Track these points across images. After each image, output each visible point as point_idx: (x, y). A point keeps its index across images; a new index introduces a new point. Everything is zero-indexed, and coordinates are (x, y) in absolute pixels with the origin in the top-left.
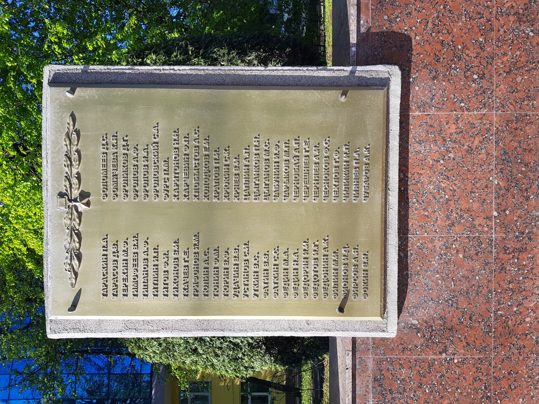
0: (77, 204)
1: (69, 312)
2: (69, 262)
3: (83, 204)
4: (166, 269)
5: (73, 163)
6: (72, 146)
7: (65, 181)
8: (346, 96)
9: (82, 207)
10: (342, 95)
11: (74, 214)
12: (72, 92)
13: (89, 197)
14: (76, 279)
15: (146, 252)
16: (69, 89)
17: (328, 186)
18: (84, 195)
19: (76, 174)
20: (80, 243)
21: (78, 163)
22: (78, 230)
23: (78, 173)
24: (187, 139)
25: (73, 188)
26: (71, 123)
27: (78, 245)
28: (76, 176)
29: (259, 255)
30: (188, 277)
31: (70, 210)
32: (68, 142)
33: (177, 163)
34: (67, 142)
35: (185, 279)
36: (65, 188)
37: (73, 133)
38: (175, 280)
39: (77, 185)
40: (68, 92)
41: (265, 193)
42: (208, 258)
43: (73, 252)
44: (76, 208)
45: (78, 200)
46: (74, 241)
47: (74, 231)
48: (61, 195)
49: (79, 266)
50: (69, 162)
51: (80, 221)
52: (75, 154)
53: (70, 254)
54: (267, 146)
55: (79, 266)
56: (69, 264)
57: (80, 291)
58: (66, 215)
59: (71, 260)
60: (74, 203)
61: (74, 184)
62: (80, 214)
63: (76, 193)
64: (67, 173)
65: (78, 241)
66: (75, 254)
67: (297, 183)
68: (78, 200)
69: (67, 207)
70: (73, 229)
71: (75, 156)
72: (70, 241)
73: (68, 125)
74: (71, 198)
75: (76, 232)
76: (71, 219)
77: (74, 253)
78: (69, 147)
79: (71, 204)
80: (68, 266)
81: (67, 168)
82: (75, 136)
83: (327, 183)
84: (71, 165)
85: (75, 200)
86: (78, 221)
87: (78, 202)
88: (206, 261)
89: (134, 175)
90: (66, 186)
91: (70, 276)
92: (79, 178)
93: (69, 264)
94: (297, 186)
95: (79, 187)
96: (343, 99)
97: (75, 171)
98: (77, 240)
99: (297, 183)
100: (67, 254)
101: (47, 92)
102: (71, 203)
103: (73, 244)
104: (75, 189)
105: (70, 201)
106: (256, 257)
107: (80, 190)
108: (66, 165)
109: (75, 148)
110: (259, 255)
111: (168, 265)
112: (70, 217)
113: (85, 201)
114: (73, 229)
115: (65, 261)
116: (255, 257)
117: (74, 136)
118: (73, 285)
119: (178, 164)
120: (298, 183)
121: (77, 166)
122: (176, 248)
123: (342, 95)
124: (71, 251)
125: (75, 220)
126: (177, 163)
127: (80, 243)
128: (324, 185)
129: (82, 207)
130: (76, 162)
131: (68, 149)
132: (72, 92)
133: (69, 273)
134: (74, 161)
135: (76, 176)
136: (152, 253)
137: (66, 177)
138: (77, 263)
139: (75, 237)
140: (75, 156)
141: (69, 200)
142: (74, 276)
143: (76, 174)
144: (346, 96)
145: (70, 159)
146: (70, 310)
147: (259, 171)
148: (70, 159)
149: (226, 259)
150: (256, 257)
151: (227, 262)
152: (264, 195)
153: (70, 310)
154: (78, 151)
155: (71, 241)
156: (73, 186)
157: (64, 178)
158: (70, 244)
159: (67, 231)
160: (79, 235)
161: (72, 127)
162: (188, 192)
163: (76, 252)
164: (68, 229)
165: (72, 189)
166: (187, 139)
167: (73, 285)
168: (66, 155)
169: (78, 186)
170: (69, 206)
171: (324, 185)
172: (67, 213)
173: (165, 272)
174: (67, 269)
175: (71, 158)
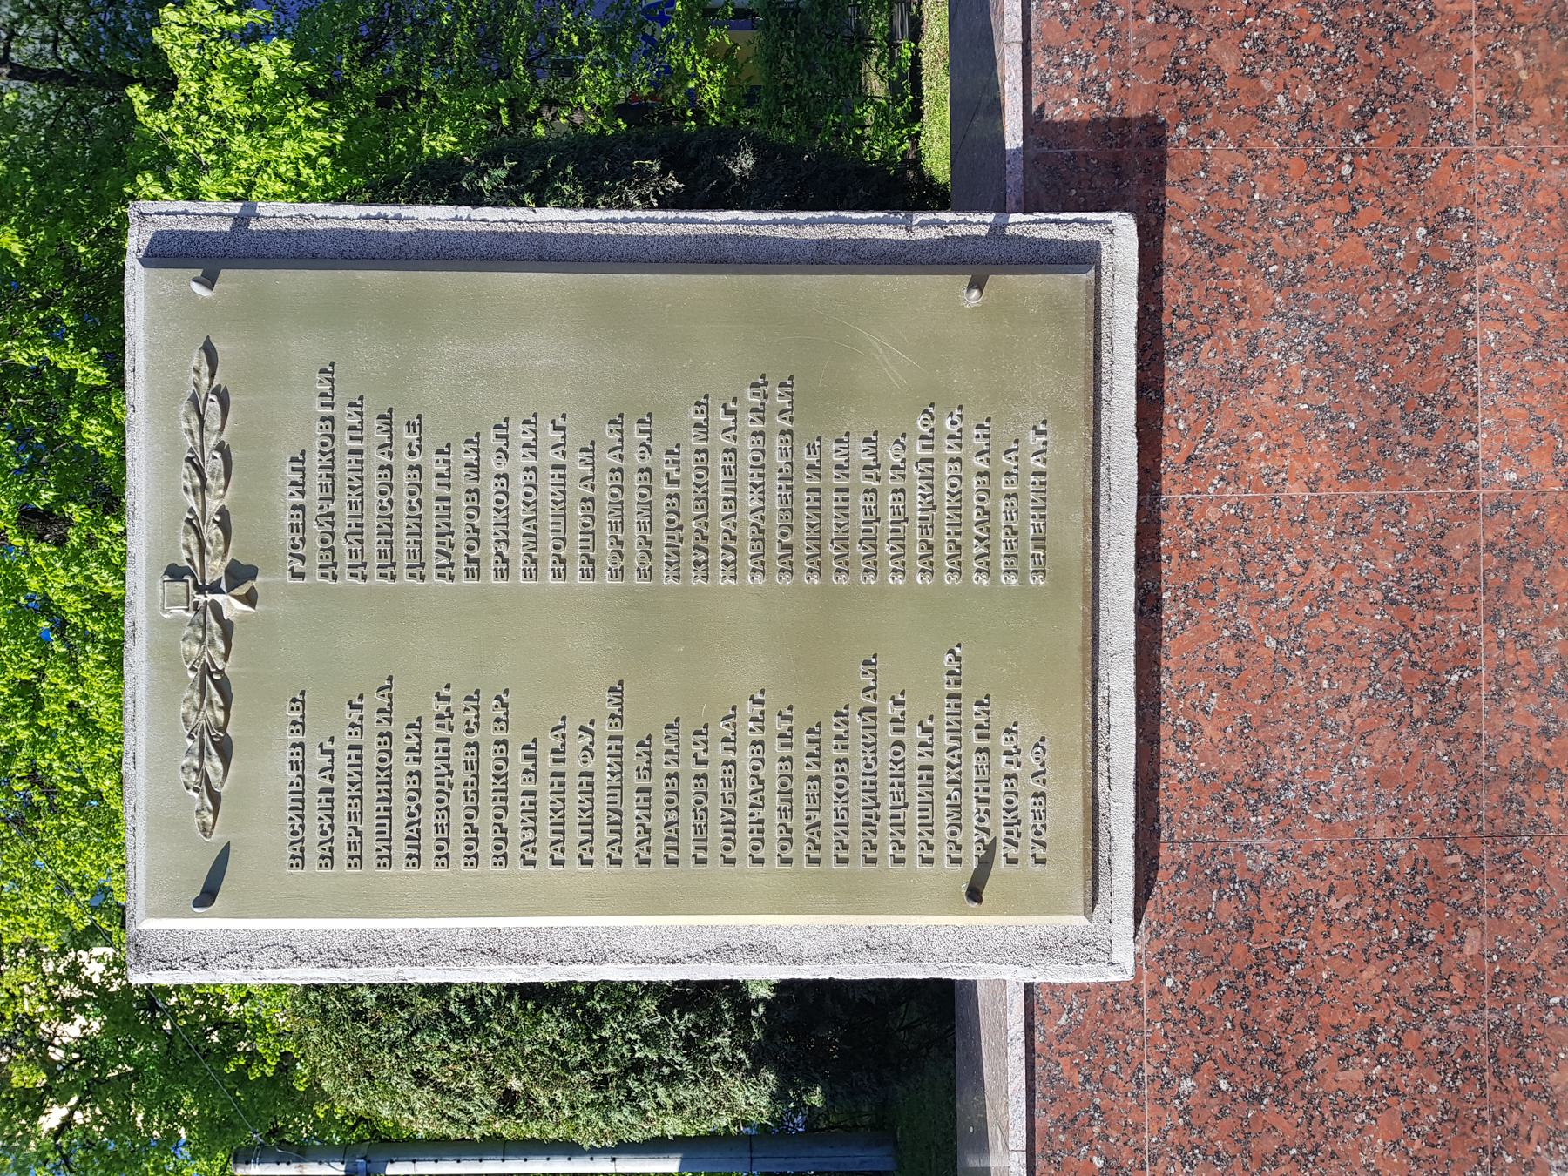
0: (219, 598)
1: (196, 910)
2: (197, 764)
5: (209, 481)
6: (205, 434)
7: (186, 532)
8: (981, 291)
9: (232, 607)
10: (970, 287)
13: (254, 578)
14: (215, 813)
16: (198, 273)
18: (238, 575)
20: (226, 709)
21: (222, 481)
22: (221, 672)
23: (222, 512)
25: (208, 554)
26: (205, 368)
27: (220, 715)
28: (218, 519)
31: (200, 615)
32: (195, 423)
36: (185, 554)
37: (211, 397)
39: (218, 544)
43: (206, 734)
44: (217, 609)
45: (223, 586)
46: (211, 703)
48: (175, 573)
49: (225, 776)
50: (197, 481)
51: (228, 646)
52: (214, 457)
53: (197, 744)
55: (225, 776)
56: (195, 770)
57: (227, 848)
58: (187, 631)
60: (210, 597)
61: (211, 541)
62: (227, 629)
63: (215, 569)
64: (191, 511)
65: (221, 704)
66: (213, 742)
68: (223, 586)
69: (191, 605)
70: (207, 671)
71: (214, 464)
72: (198, 704)
74: (203, 581)
75: (216, 677)
76: (201, 642)
77: (212, 738)
78: (197, 435)
79: (201, 599)
80: (194, 777)
82: (216, 405)
84: (204, 486)
85: (215, 588)
86: (221, 645)
87: (223, 592)
91: (198, 805)
92: (224, 524)
93: (195, 770)
97: (213, 505)
98: (217, 699)
100: (190, 742)
102: (202, 596)
103: (209, 713)
104: (216, 557)
105: (200, 589)
108: (190, 488)
109: (212, 441)
112: (200, 634)
113: (242, 590)
114: (207, 671)
117: (213, 407)
121: (221, 492)
123: (970, 287)
124: (202, 733)
125: (212, 644)
127: (226, 709)
129: (232, 607)
130: (218, 479)
132: (209, 281)
133: (196, 795)
135: (218, 519)
138: (219, 766)
139: (214, 691)
140: (214, 464)
141: (196, 585)
144: (981, 291)
146: (198, 903)
154: (221, 448)
155: (201, 705)
156: (208, 545)
159: (192, 675)
160: (224, 688)
161: (207, 380)
163: (217, 736)
164: (192, 669)
165: (206, 557)
168: (189, 460)
169: (221, 548)
170: (196, 604)
174: (191, 784)
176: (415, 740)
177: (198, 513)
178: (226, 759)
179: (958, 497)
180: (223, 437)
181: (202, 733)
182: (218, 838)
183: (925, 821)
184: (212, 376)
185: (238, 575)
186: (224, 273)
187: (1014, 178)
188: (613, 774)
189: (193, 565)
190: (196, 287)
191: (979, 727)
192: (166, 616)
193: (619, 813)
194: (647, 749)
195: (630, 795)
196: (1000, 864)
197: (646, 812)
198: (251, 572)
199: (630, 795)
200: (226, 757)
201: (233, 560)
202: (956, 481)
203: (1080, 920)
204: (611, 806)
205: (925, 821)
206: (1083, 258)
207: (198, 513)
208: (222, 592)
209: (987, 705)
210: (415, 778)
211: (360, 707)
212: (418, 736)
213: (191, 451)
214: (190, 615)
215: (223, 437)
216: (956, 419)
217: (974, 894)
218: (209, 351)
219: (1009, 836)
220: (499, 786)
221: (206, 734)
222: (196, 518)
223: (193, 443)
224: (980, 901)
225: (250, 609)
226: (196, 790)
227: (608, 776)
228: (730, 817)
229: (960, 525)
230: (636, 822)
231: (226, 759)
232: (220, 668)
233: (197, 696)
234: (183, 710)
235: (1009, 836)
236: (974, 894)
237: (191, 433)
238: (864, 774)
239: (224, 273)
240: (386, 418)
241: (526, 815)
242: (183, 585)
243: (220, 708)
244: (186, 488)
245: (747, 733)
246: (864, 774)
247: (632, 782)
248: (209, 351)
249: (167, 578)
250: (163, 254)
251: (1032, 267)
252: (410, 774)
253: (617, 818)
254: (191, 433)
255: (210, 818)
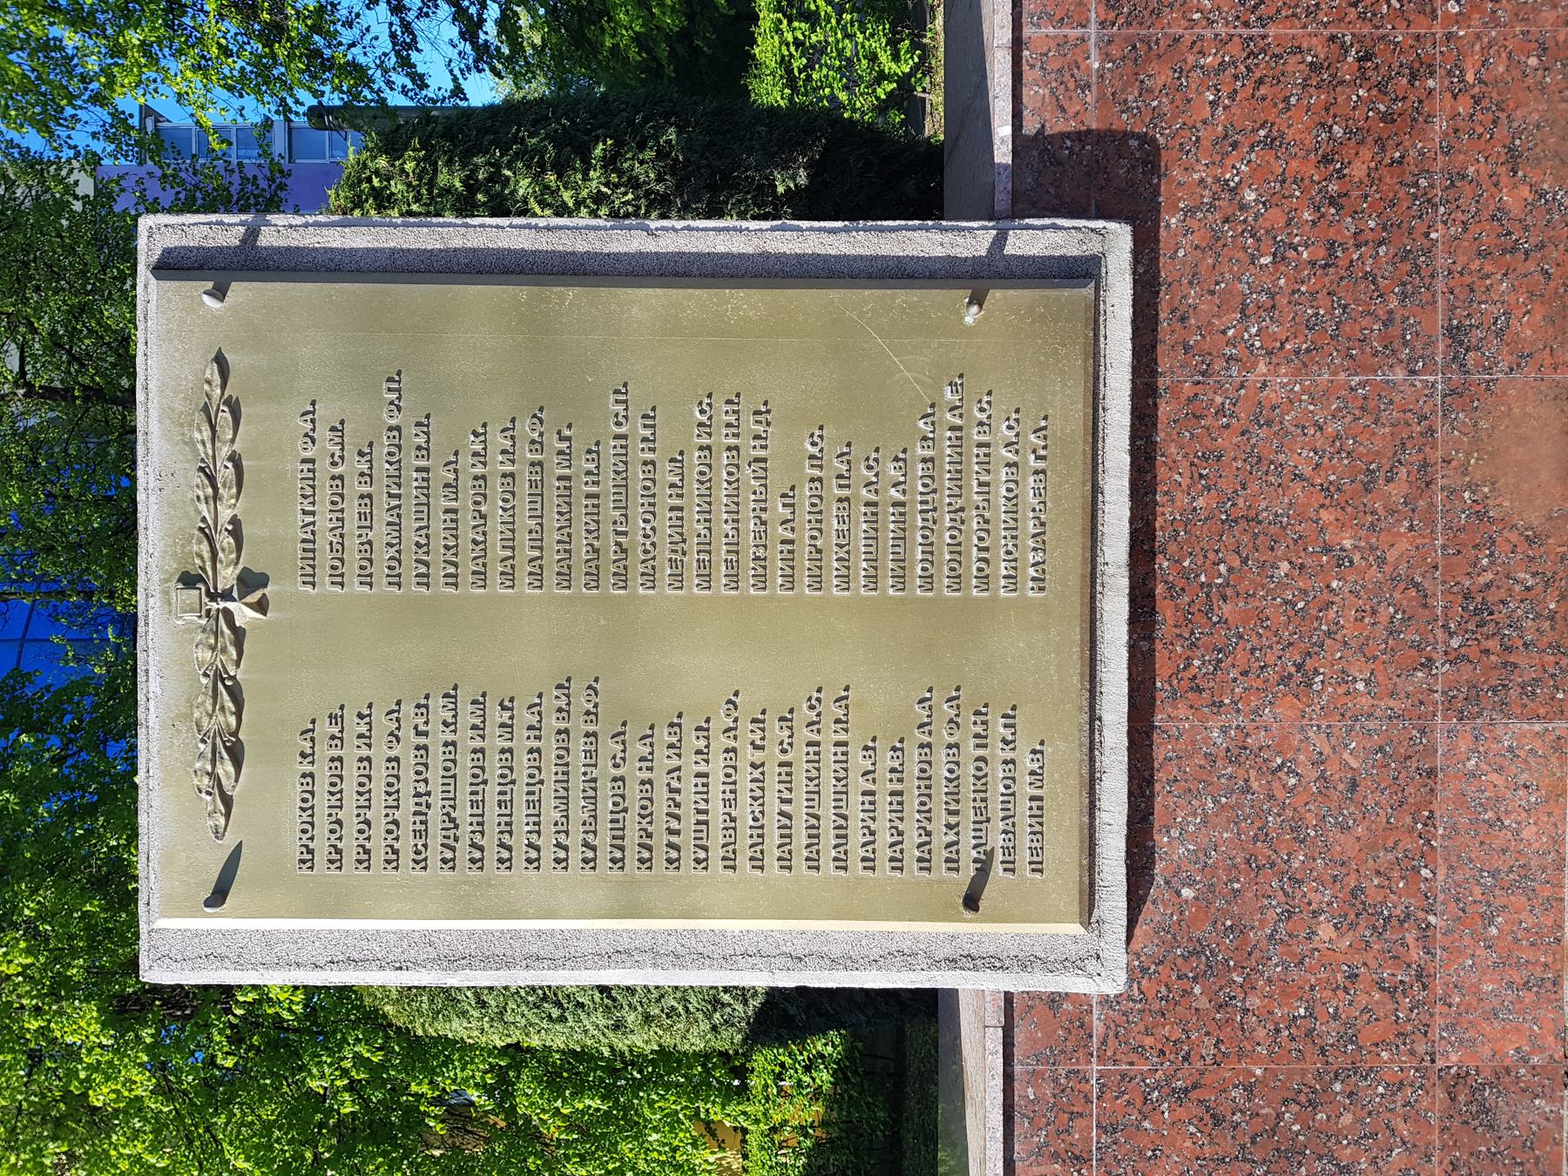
0: (230, 605)
1: (207, 910)
2: (209, 768)
3: (248, 605)
4: (392, 753)
5: (221, 491)
6: (218, 444)
7: (200, 542)
9: (243, 614)
11: (222, 632)
12: (219, 293)
13: (265, 586)
14: (227, 815)
15: (393, 711)
16: (209, 285)
17: (1015, 545)
18: (250, 582)
19: (229, 523)
21: (234, 490)
22: (233, 678)
23: (235, 521)
24: (396, 386)
25: (221, 562)
26: (217, 380)
27: (232, 720)
28: (230, 528)
29: (821, 696)
30: (595, 766)
31: (213, 622)
32: (207, 434)
33: (650, 504)
34: (205, 434)
35: (589, 770)
36: (198, 561)
38: (333, 784)
39: (231, 552)
40: (205, 293)
41: (699, 535)
42: (819, 715)
43: (218, 739)
44: (229, 616)
45: (235, 594)
46: (223, 709)
47: (223, 680)
48: (189, 580)
50: (210, 491)
51: (240, 653)
52: (226, 467)
53: (209, 749)
54: (816, 444)
55: (237, 780)
56: (208, 773)
58: (200, 637)
59: (214, 766)
60: (222, 605)
61: (223, 550)
62: (239, 635)
63: (227, 576)
64: (204, 520)
65: (233, 709)
66: (225, 747)
67: (761, 509)
68: (235, 594)
69: (203, 613)
70: (219, 677)
71: (226, 473)
72: (210, 708)
73: (206, 387)
74: (216, 588)
75: (229, 683)
76: (213, 648)
77: (224, 742)
78: (209, 445)
79: (214, 606)
80: (206, 780)
81: (203, 507)
82: (228, 415)
83: (1013, 537)
84: (216, 496)
85: (227, 595)
86: (233, 651)
87: (235, 600)
88: (393, 711)
89: (333, 503)
90: (202, 558)
91: (210, 808)
92: (236, 532)
93: (208, 773)
94: (760, 518)
95: (238, 557)
96: (971, 316)
97: (225, 514)
98: (230, 705)
99: (761, 509)
100: (202, 746)
101: (148, 289)
102: (214, 604)
103: (221, 718)
104: (228, 565)
105: (213, 597)
106: (813, 702)
107: (240, 566)
108: (202, 497)
109: (225, 451)
110: (821, 696)
111: (398, 742)
112: (212, 641)
113: (254, 597)
114: (219, 677)
115: (198, 765)
116: (810, 699)
117: (225, 416)
118: (219, 834)
119: (653, 505)
120: (764, 510)
121: (233, 501)
122: (563, 703)
123: (970, 303)
124: (214, 737)
125: (224, 650)
126: (650, 504)
128: (1003, 542)
129: (243, 614)
131: (206, 454)
132: (219, 293)
133: (209, 798)
134: (224, 485)
135: (230, 528)
136: (467, 718)
137: (202, 530)
138: (231, 769)
139: (226, 697)
140: (226, 473)
141: (208, 593)
142: (222, 808)
143: (229, 523)
144: (981, 306)
145: (212, 480)
146: (209, 903)
147: (737, 496)
148: (212, 480)
149: (590, 706)
150: (813, 702)
151: (593, 717)
152: (696, 540)
153: (209, 903)
154: (235, 459)
155: (214, 710)
156: (221, 555)
157: (196, 532)
158: (211, 716)
159: (204, 681)
160: (236, 694)
161: (219, 391)
162: (427, 536)
164: (206, 675)
165: (218, 565)
166: (396, 386)
167: (219, 834)
168: (201, 469)
169: (233, 556)
170: (209, 611)
171: (1003, 542)
172: (204, 631)
173: (389, 760)
174: (204, 788)
175: (215, 478)
176: (703, 743)
177: (210, 522)
178: (238, 765)
179: (1014, 501)
180: (235, 447)
181: (214, 737)
182: (230, 842)
183: (616, 825)
184: (224, 386)
185: (250, 582)
186: (234, 285)
187: (1003, 186)
188: (838, 780)
189: (206, 573)
190: (206, 298)
191: (977, 736)
192: (179, 623)
193: (845, 818)
194: (705, 757)
195: (856, 798)
196: (997, 869)
197: (871, 815)
198: (263, 581)
199: (856, 798)
200: (237, 758)
201: (245, 568)
202: (1012, 486)
203: (1077, 929)
204: (838, 811)
205: (616, 825)
206: (1084, 271)
207: (210, 522)
208: (234, 600)
209: (986, 714)
210: (309, 780)
211: (511, 709)
212: (707, 738)
213: (203, 460)
214: (203, 622)
215: (235, 447)
216: (1012, 423)
217: (971, 901)
218: (220, 360)
219: (446, 841)
220: (979, 787)
221: (218, 739)
222: (209, 527)
223: (206, 454)
224: (977, 910)
225: (261, 616)
226: (209, 793)
227: (834, 781)
228: (785, 821)
229: (1016, 529)
230: (861, 824)
231: (238, 765)
232: (232, 674)
233: (209, 702)
234: (196, 715)
235: (446, 841)
236: (971, 901)
237: (203, 443)
238: (724, 783)
239: (234, 285)
240: (338, 430)
241: (1034, 820)
242: (197, 592)
243: (232, 713)
244: (198, 497)
245: (720, 742)
246: (724, 783)
247: (858, 784)
248: (220, 360)
249: (180, 586)
250: (172, 266)
251: (951, 281)
252: (304, 776)
253: (843, 822)
254: (203, 443)
255: (222, 821)
